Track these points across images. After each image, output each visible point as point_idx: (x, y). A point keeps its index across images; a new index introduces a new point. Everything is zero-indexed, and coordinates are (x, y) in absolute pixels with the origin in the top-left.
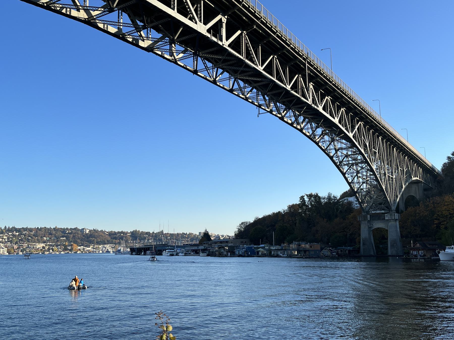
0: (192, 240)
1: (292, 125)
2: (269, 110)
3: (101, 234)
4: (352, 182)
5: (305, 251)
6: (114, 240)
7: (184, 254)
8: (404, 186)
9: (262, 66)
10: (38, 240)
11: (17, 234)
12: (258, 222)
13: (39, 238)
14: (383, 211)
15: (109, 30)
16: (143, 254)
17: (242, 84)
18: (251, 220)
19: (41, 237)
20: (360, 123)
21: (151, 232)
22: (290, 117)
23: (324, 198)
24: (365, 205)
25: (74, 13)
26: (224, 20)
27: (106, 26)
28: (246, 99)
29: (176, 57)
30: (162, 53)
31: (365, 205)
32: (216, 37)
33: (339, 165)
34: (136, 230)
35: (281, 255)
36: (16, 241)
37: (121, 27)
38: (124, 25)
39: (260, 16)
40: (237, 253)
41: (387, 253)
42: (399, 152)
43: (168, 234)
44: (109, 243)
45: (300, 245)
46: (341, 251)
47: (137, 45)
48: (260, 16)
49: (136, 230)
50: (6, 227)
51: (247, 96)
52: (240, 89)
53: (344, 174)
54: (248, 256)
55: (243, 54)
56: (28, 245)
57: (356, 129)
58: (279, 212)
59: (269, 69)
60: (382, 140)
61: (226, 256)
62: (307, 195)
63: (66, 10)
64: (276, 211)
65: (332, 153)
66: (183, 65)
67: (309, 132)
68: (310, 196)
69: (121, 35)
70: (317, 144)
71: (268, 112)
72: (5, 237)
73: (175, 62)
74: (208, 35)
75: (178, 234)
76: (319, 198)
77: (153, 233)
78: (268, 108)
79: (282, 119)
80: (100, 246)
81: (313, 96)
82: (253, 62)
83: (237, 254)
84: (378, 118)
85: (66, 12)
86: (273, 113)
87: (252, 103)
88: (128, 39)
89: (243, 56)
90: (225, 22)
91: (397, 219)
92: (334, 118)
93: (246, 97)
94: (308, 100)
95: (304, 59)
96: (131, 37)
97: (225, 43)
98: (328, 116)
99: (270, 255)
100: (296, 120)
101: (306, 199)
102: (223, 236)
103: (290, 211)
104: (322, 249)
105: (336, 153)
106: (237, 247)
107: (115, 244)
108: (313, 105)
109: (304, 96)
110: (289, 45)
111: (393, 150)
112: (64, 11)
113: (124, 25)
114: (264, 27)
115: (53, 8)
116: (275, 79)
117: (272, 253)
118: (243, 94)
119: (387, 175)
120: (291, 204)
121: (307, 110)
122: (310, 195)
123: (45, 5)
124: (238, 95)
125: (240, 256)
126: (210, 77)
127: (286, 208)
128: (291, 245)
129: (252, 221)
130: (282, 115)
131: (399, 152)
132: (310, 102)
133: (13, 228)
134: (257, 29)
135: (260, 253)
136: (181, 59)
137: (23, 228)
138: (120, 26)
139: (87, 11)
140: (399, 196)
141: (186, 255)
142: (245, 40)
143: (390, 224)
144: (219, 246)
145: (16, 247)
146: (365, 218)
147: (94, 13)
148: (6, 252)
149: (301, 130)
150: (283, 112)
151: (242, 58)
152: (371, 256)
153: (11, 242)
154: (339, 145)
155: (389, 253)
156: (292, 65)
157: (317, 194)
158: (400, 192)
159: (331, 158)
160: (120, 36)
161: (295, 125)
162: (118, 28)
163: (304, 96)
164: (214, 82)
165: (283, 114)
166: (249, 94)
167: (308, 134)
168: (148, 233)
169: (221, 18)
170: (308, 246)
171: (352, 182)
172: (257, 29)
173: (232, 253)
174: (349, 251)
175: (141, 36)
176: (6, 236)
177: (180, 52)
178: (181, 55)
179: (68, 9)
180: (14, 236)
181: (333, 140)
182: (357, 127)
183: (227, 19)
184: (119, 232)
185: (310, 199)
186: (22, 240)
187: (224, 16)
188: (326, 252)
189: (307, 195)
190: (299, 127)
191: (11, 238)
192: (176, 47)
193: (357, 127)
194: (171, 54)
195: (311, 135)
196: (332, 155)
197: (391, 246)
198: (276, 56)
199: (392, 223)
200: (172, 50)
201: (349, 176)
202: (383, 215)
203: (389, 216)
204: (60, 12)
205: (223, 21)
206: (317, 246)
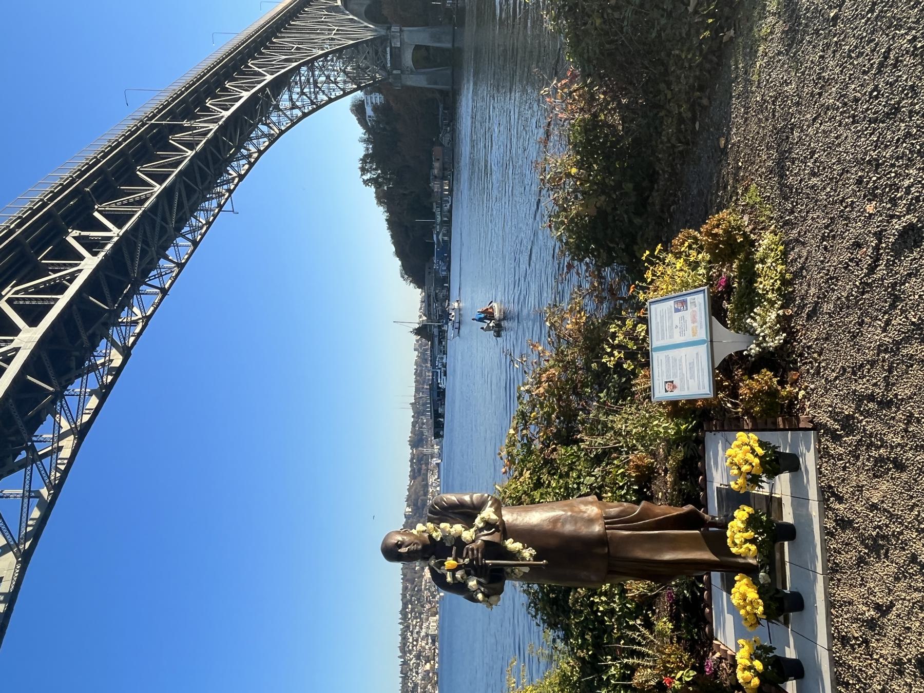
0: (425, 361)
1: (251, 165)
2: (227, 194)
3: (413, 490)
4: (343, 90)
5: (444, 169)
6: (423, 472)
7: (445, 356)
8: (351, 17)
9: (81, 258)
10: (419, 578)
11: (410, 606)
12: (400, 253)
13: (417, 575)
14: (388, 49)
15: (94, 407)
16: (442, 420)
17: (186, 229)
18: (398, 263)
19: (416, 573)
20: (249, 64)
21: (412, 420)
22: (239, 166)
23: (367, 149)
24: (378, 76)
25: (66, 453)
26: (76, 233)
27: (87, 411)
28: (209, 224)
29: (140, 316)
30: (132, 336)
31: (378, 76)
32: (106, 244)
33: (316, 105)
34: (409, 441)
35: (448, 205)
36: (420, 608)
37: (88, 390)
38: (84, 385)
39: (68, 179)
40: (444, 273)
41: (448, 50)
42: (298, 17)
43: (415, 396)
44: (425, 479)
45: (436, 177)
46: (445, 119)
47: (119, 370)
48: (68, 179)
49: (409, 441)
50: (400, 623)
51: (204, 222)
52: (193, 231)
53: (331, 100)
54: (449, 256)
55: (133, 211)
56: (426, 589)
57: (260, 70)
58: (387, 220)
59: (160, 178)
60: (277, 37)
61: (448, 289)
62: (362, 175)
63: (60, 464)
64: (385, 225)
65: (298, 113)
66: (152, 308)
67: (264, 142)
68: (364, 170)
69: (101, 390)
70: (282, 132)
71: (230, 196)
72: (414, 623)
73: (147, 319)
74: (101, 255)
75: (415, 382)
76: (366, 156)
77: (413, 417)
78: (224, 195)
79: (241, 177)
80: (431, 491)
81: (205, 122)
82: (147, 199)
83: (445, 273)
84: (242, 37)
85: (64, 464)
86: (232, 188)
87: (215, 216)
88: (109, 381)
89: (136, 211)
90: (78, 232)
91: (401, 29)
92: (241, 97)
93: (206, 224)
94: (211, 130)
95: (143, 125)
96: (105, 377)
97: (115, 233)
98: (237, 105)
99: (448, 223)
100: (244, 157)
101: (368, 176)
102: (420, 317)
103: (384, 202)
104: (442, 145)
105: (297, 107)
106: (437, 272)
107: (427, 470)
108: (220, 123)
109: (205, 134)
110: (119, 144)
111: (294, 25)
112: (62, 467)
113: (84, 385)
114: (88, 174)
115: (57, 482)
116: (177, 171)
117: (446, 219)
118: (201, 228)
119: (332, 36)
120: (375, 202)
121: (228, 135)
122: (362, 171)
123: (52, 492)
124: (203, 235)
125: (449, 269)
126: (172, 272)
127: (381, 209)
128: (436, 190)
129: (400, 263)
130: (236, 177)
131: (298, 17)
132: (214, 127)
133: (401, 612)
134: (90, 187)
135: (446, 238)
136: (143, 309)
137: (402, 600)
138: (85, 392)
139: (62, 437)
140: (366, 24)
141: (445, 353)
142: (112, 206)
143: (406, 40)
144: (434, 302)
145: (427, 606)
146: (398, 77)
147: (65, 426)
148: (435, 618)
149: (261, 153)
150: (231, 175)
151: (140, 212)
152: (453, 74)
153: (421, 613)
154: (288, 104)
155: (449, 45)
156: (154, 146)
157: (361, 160)
158: (359, 22)
159: (305, 115)
160: (104, 393)
161: (252, 160)
162: (91, 395)
163: (205, 134)
164: (181, 266)
165: (235, 175)
166: (201, 220)
167: (267, 143)
168: (414, 424)
169: (73, 237)
170: (437, 165)
171: (343, 90)
172: (90, 187)
173: (443, 282)
174: (445, 108)
175: (103, 364)
176: (412, 621)
177: (130, 312)
178: (136, 310)
179: (59, 461)
180: (412, 610)
181: (277, 108)
182: (257, 69)
183: (73, 229)
184: (411, 466)
185: (368, 171)
186: (418, 600)
187: (69, 233)
188: (446, 140)
189: (362, 175)
190: (255, 155)
191: (415, 614)
192: (124, 317)
193: (257, 69)
194: (135, 323)
195: (269, 139)
196: (300, 114)
197: (439, 42)
198: (138, 168)
199: (406, 36)
200: (127, 322)
201: (333, 94)
202: (393, 50)
203: (395, 40)
204: (65, 473)
205: (77, 235)
206: (437, 150)
